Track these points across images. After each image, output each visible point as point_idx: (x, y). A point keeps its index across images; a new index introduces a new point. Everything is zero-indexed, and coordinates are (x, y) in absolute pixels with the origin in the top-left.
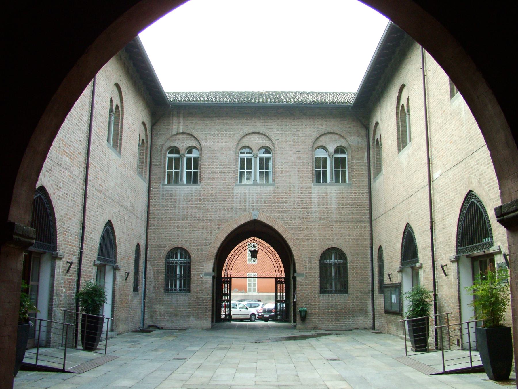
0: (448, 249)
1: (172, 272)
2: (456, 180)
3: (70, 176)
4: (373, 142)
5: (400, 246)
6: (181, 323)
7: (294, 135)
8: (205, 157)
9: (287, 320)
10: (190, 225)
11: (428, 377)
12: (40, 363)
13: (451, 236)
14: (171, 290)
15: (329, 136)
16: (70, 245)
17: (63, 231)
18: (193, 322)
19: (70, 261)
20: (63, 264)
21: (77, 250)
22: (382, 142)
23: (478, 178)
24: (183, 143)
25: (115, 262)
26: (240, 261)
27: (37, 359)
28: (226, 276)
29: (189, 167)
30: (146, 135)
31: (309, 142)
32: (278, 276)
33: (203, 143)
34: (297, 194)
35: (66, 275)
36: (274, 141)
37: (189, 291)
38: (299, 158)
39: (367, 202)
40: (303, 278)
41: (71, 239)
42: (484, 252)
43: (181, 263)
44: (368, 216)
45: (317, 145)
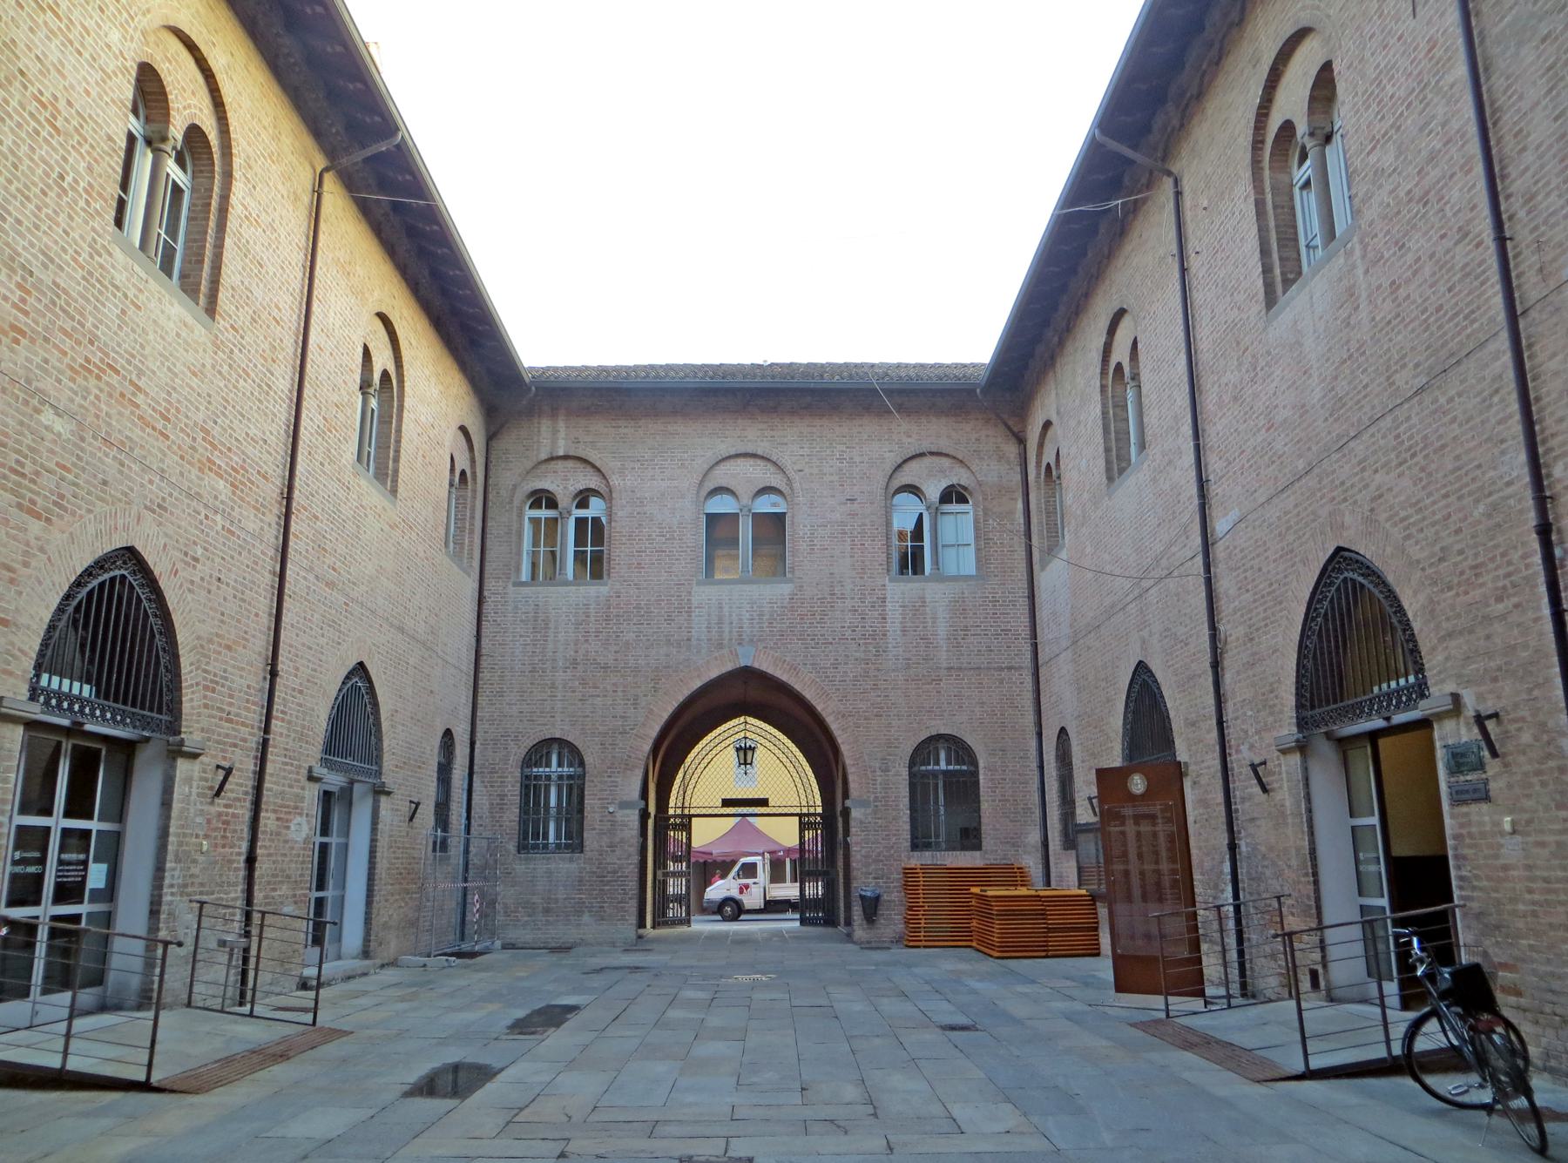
0: (1271, 719)
1: (536, 803)
2: (1288, 529)
3: (233, 533)
4: (1038, 474)
5: (1121, 723)
6: (562, 932)
7: (841, 460)
8: (620, 514)
9: (830, 921)
10: (584, 683)
11: (1261, 1089)
12: (74, 1064)
13: (1279, 681)
14: (535, 847)
15: (928, 460)
16: (230, 721)
17: (205, 679)
18: (588, 927)
19: (226, 764)
20: (204, 771)
21: (253, 735)
22: (1062, 466)
23: (1367, 507)
24: (564, 483)
25: (379, 773)
26: (711, 773)
27: (66, 1053)
28: (679, 812)
29: (580, 541)
30: (473, 461)
31: (880, 479)
32: (805, 810)
33: (615, 481)
34: (849, 603)
35: (212, 803)
36: (792, 474)
37: (580, 848)
38: (853, 515)
39: (1025, 620)
40: (869, 811)
41: (231, 704)
42: (1388, 719)
43: (560, 777)
44: (1028, 655)
45: (896, 483)
